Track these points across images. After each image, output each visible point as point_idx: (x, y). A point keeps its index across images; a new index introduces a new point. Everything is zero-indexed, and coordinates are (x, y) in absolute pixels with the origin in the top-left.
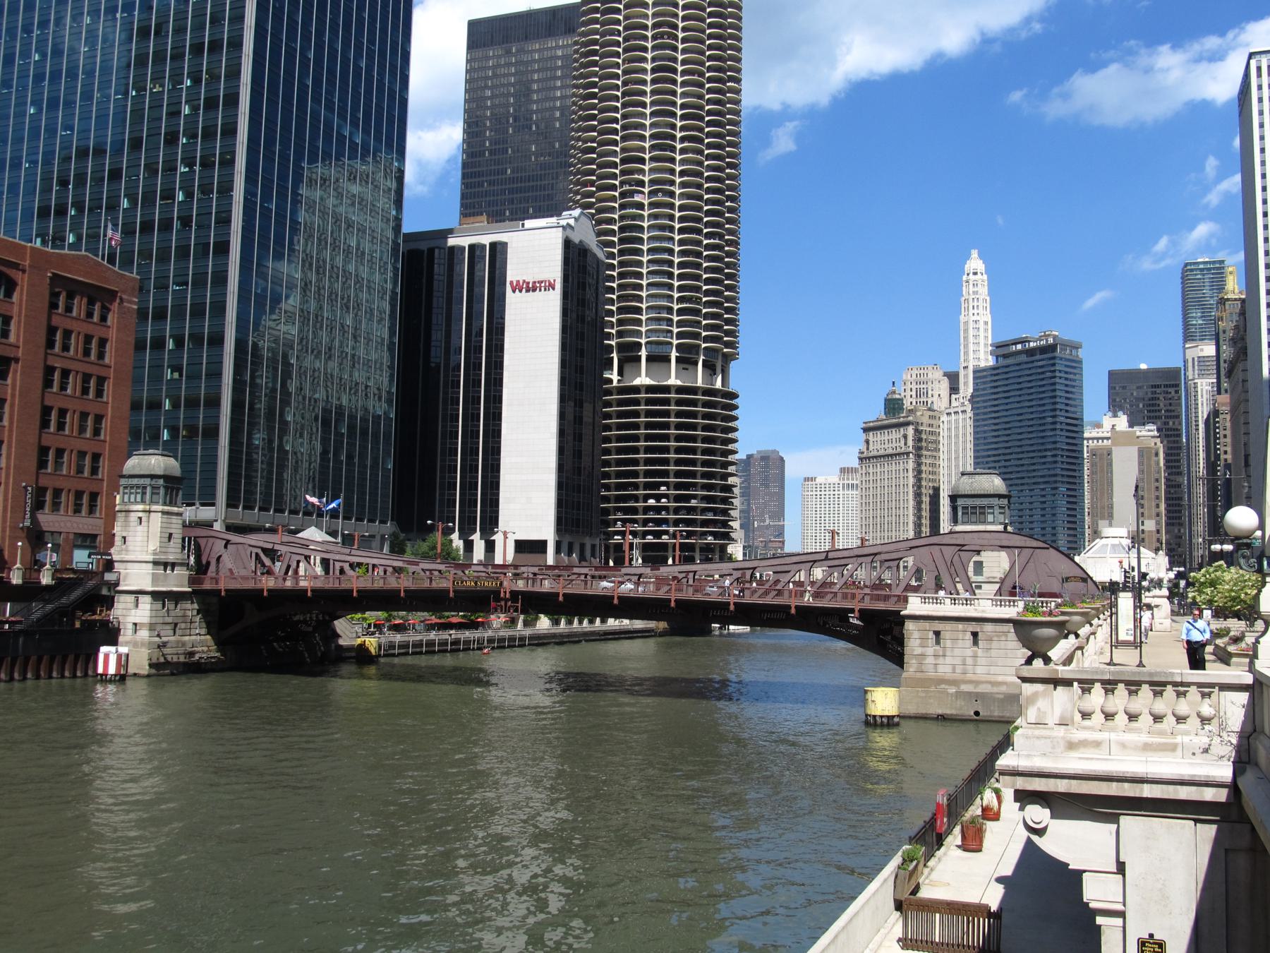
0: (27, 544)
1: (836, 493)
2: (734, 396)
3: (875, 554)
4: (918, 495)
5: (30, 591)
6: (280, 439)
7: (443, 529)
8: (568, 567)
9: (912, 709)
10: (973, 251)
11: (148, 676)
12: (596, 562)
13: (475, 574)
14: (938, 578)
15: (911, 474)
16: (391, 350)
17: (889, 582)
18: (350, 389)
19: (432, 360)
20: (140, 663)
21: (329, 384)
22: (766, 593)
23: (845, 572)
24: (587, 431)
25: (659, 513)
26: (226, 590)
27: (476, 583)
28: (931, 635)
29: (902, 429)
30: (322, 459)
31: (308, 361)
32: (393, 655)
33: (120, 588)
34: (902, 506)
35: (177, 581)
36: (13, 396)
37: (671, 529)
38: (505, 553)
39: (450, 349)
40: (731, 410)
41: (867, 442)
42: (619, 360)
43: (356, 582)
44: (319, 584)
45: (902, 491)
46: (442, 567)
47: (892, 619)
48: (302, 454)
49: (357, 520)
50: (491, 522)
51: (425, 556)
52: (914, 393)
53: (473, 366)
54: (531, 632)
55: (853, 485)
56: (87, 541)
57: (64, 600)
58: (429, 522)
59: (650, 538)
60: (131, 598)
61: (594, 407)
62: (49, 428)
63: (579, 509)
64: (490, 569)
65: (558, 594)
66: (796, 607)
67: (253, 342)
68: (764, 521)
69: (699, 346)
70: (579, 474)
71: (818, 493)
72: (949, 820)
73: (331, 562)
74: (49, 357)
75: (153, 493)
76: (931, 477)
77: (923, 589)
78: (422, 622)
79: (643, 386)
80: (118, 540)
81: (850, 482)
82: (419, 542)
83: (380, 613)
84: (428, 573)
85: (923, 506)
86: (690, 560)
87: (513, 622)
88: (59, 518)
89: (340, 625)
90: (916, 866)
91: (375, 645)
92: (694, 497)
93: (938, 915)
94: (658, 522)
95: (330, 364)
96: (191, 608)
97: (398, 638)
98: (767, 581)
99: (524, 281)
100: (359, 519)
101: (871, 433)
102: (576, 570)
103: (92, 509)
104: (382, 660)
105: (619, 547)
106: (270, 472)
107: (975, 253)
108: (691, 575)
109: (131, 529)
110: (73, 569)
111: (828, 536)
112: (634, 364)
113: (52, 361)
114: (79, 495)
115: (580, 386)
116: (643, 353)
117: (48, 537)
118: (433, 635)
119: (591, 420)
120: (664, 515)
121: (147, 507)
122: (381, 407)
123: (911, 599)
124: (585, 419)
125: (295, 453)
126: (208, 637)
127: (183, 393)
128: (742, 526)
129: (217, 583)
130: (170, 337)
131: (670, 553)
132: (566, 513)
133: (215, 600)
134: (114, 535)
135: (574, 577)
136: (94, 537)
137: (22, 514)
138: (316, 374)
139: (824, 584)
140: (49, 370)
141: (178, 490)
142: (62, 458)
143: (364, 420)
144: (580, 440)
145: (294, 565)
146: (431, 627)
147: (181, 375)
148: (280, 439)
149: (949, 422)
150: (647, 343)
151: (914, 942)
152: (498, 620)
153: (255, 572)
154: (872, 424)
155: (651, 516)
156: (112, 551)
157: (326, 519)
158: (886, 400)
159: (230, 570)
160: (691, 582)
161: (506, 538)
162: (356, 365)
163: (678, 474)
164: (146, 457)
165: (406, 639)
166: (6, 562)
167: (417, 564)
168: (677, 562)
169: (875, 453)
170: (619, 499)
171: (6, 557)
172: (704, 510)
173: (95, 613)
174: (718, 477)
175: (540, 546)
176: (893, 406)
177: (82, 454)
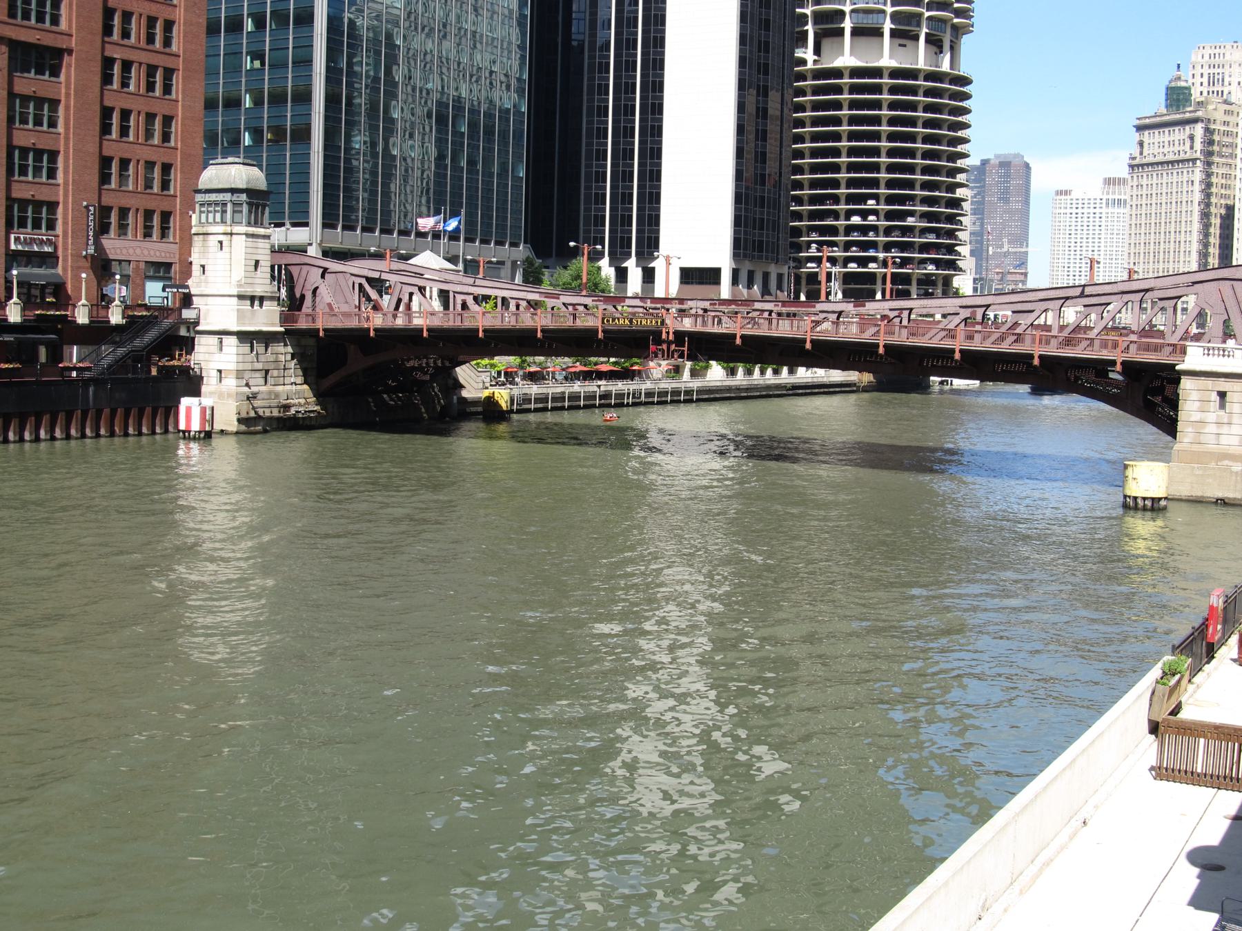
0: (93, 277)
1: (1097, 211)
2: (965, 81)
3: (1147, 291)
4: (1205, 215)
5: (98, 332)
6: (386, 140)
7: (589, 253)
8: (748, 302)
9: (1184, 491)
11: (237, 433)
12: (783, 296)
13: (630, 310)
14: (1226, 323)
15: (1197, 187)
16: (521, 24)
17: (1162, 328)
18: (471, 76)
19: (574, 37)
20: (227, 419)
21: (444, 70)
22: (1002, 338)
23: (1105, 314)
24: (773, 128)
25: (865, 235)
26: (325, 330)
27: (631, 321)
28: (1214, 397)
29: (1187, 128)
30: (437, 166)
31: (418, 42)
32: (529, 411)
33: (199, 328)
34: (1183, 230)
35: (268, 319)
36: (68, 95)
37: (881, 255)
38: (667, 283)
39: (595, 24)
40: (962, 100)
41: (1141, 144)
42: (816, 34)
43: (482, 319)
44: (436, 322)
45: (1184, 209)
46: (588, 301)
47: (1164, 375)
48: (413, 160)
49: (482, 242)
50: (649, 245)
51: (567, 288)
52: (1205, 80)
53: (625, 44)
54: (699, 384)
55: (1119, 200)
56: (160, 270)
57: (137, 343)
58: (572, 244)
59: (853, 267)
60: (214, 340)
61: (783, 95)
62: (110, 133)
63: (762, 228)
64: (649, 304)
65: (734, 336)
66: (1040, 357)
67: (350, 19)
68: (1002, 246)
69: (920, 15)
70: (763, 183)
71: (1074, 211)
72: (1223, 629)
73: (451, 295)
74: (107, 45)
75: (234, 212)
76: (1223, 191)
77: (1206, 337)
78: (563, 370)
79: (846, 68)
80: (196, 269)
81: (1117, 197)
82: (559, 270)
83: (512, 358)
84: (570, 308)
85: (1212, 230)
86: (905, 295)
87: (677, 370)
88: (127, 243)
89: (464, 373)
90: (1179, 681)
91: (506, 397)
92: (912, 214)
93: (1202, 740)
94: (865, 246)
95: (446, 44)
96: (283, 351)
97: (534, 389)
98: (1003, 323)
100: (485, 241)
101: (1146, 133)
102: (758, 306)
103: (164, 234)
104: (515, 416)
105: (813, 278)
106: (375, 183)
108: (905, 314)
109: (210, 256)
110: (145, 305)
111: (1085, 269)
112: (836, 39)
113: (112, 52)
114: (149, 214)
115: (764, 69)
116: (847, 25)
117: (115, 267)
118: (577, 387)
119: (778, 113)
120: (871, 237)
121: (228, 229)
122: (510, 98)
123: (1189, 349)
124: (770, 112)
125: (405, 159)
126: (306, 387)
127: (266, 87)
128: (972, 253)
129: (314, 321)
130: (249, 15)
131: (879, 286)
132: (746, 233)
133: (311, 342)
134: (191, 263)
135: (755, 314)
136: (168, 266)
137: (85, 240)
138: (428, 58)
139: (1077, 328)
140: (108, 63)
141: (264, 206)
142: (127, 170)
143: (489, 116)
144: (764, 139)
145: (406, 298)
146: (571, 377)
147: (263, 64)
148: (386, 140)
150: (853, 11)
151: (1170, 771)
152: (658, 368)
153: (359, 308)
154: (1147, 121)
155: (856, 237)
156: (190, 282)
157: (444, 241)
158: (1167, 88)
159: (329, 305)
160: (905, 322)
161: (668, 264)
162: (478, 45)
163: (891, 184)
164: (225, 167)
165: (545, 391)
166: (69, 298)
167: (557, 297)
168: (888, 297)
169: (1151, 159)
170: (813, 215)
171: (69, 292)
172: (924, 231)
173: (173, 358)
174: (944, 188)
175: (709, 276)
176: (1177, 96)
177: (150, 165)
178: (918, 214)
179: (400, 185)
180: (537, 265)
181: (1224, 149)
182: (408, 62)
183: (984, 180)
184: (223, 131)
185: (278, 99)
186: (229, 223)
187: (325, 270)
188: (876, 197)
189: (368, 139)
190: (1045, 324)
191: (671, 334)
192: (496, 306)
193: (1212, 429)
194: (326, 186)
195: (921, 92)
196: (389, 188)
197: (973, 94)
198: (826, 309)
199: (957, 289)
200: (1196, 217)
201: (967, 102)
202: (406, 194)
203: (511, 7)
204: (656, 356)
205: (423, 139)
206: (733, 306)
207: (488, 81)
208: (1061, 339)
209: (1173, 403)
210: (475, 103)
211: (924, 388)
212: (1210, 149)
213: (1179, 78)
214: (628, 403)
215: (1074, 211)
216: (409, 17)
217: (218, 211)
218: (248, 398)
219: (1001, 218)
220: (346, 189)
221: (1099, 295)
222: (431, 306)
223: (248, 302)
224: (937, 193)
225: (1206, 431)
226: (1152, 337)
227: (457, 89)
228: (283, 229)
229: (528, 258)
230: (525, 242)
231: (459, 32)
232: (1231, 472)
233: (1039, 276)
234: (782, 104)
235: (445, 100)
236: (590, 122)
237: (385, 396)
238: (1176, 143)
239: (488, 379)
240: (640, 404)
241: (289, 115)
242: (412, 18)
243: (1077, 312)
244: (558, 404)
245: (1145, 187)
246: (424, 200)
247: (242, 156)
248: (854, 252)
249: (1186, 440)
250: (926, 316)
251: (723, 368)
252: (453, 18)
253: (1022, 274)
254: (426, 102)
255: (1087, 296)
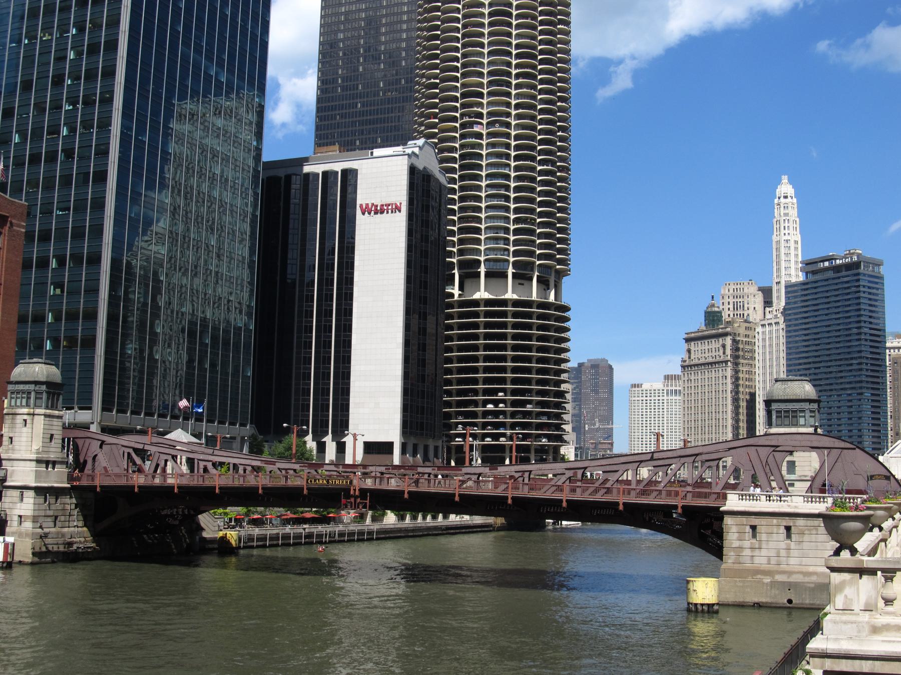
2: (566, 309)
3: (697, 455)
4: (736, 400)
6: (151, 348)
7: (298, 432)
8: (413, 467)
9: (730, 598)
10: (783, 177)
12: (438, 462)
16: (251, 267)
17: (709, 480)
18: (214, 303)
20: (24, 552)
21: (195, 299)
22: (596, 491)
23: (669, 471)
26: (101, 487)
27: (328, 481)
29: (720, 339)
30: (188, 368)
31: (176, 278)
32: (252, 547)
33: (7, 484)
34: (721, 410)
37: (508, 432)
38: (354, 454)
39: (305, 267)
40: (563, 322)
41: (689, 351)
43: (218, 480)
44: (184, 482)
45: (721, 396)
46: (297, 467)
49: (220, 423)
50: (342, 426)
51: (281, 457)
52: (731, 306)
53: (325, 282)
54: (378, 527)
60: (16, 493)
61: (437, 319)
64: (341, 469)
66: (624, 504)
67: (127, 261)
68: (594, 424)
69: (534, 263)
70: (424, 381)
71: (644, 398)
73: (196, 461)
75: (36, 398)
76: (747, 383)
77: (740, 487)
78: (278, 517)
79: (482, 300)
81: (674, 388)
83: (240, 508)
84: (284, 472)
85: (741, 410)
86: (526, 461)
87: (362, 517)
89: (204, 519)
91: (235, 537)
92: (530, 402)
95: (196, 281)
96: (69, 502)
97: (256, 531)
98: (597, 480)
99: (373, 204)
101: (692, 343)
102: (420, 470)
104: (242, 552)
105: (460, 448)
106: (141, 379)
107: (785, 179)
108: (527, 474)
109: (17, 430)
115: (424, 301)
116: (482, 270)
118: (288, 529)
119: (434, 331)
120: (501, 419)
121: (32, 411)
123: (729, 496)
124: (428, 330)
125: (164, 362)
126: (85, 529)
127: (64, 308)
128: (574, 429)
129: (93, 480)
134: (2, 435)
138: (184, 290)
139: (650, 482)
141: (59, 395)
143: (226, 332)
144: (424, 350)
145: (162, 464)
146: (286, 522)
147: (62, 292)
148: (151, 348)
149: (764, 333)
150: (486, 260)
152: (348, 515)
155: (490, 419)
157: (191, 422)
158: (706, 312)
159: (105, 468)
160: (526, 481)
161: (355, 440)
162: (220, 282)
164: (31, 365)
165: (264, 532)
167: (273, 463)
168: (514, 462)
169: (696, 362)
170: (460, 404)
172: (539, 415)
175: (385, 448)
176: (712, 317)
178: (534, 402)
179: (160, 381)
180: (259, 440)
181: (746, 354)
182: (169, 292)
183: (581, 377)
184: (30, 339)
185: (72, 317)
186: (32, 406)
187: (103, 443)
188: (504, 390)
189: (138, 347)
190: (627, 479)
191: (357, 490)
192: (229, 470)
193: (747, 552)
194: (105, 380)
195: (534, 338)
196: (153, 383)
197: (571, 328)
198: (469, 472)
199: (564, 456)
200: (729, 401)
201: (568, 323)
202: (164, 387)
203: (244, 255)
204: (346, 507)
205: (178, 348)
206: (402, 470)
207: (226, 307)
208: (638, 491)
209: (719, 534)
210: (217, 323)
211: (542, 527)
212: (737, 354)
213: (713, 306)
214: (326, 541)
215: (644, 398)
216: (170, 261)
217: (24, 398)
218: (41, 537)
219: (593, 404)
220: (120, 383)
221: (663, 459)
222: (181, 469)
223: (44, 465)
224: (548, 388)
225: (744, 554)
226: (703, 487)
227: (203, 312)
228: (73, 411)
229: (253, 435)
230: (251, 423)
231: (206, 272)
232: (764, 583)
233: (621, 446)
234: (437, 325)
235: (194, 320)
236: (299, 338)
237: (145, 536)
238: (714, 350)
239: (222, 524)
240: (335, 542)
241: (80, 329)
242: (173, 262)
243: (649, 470)
244: (275, 542)
245: (693, 381)
246: (177, 392)
247: (44, 357)
248: (489, 430)
249: (729, 561)
250: (542, 475)
251: (395, 515)
252: (202, 262)
253: (609, 443)
254: (181, 321)
255: (655, 460)
